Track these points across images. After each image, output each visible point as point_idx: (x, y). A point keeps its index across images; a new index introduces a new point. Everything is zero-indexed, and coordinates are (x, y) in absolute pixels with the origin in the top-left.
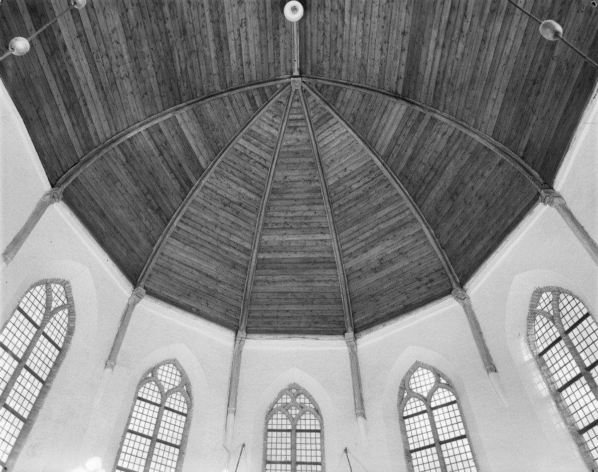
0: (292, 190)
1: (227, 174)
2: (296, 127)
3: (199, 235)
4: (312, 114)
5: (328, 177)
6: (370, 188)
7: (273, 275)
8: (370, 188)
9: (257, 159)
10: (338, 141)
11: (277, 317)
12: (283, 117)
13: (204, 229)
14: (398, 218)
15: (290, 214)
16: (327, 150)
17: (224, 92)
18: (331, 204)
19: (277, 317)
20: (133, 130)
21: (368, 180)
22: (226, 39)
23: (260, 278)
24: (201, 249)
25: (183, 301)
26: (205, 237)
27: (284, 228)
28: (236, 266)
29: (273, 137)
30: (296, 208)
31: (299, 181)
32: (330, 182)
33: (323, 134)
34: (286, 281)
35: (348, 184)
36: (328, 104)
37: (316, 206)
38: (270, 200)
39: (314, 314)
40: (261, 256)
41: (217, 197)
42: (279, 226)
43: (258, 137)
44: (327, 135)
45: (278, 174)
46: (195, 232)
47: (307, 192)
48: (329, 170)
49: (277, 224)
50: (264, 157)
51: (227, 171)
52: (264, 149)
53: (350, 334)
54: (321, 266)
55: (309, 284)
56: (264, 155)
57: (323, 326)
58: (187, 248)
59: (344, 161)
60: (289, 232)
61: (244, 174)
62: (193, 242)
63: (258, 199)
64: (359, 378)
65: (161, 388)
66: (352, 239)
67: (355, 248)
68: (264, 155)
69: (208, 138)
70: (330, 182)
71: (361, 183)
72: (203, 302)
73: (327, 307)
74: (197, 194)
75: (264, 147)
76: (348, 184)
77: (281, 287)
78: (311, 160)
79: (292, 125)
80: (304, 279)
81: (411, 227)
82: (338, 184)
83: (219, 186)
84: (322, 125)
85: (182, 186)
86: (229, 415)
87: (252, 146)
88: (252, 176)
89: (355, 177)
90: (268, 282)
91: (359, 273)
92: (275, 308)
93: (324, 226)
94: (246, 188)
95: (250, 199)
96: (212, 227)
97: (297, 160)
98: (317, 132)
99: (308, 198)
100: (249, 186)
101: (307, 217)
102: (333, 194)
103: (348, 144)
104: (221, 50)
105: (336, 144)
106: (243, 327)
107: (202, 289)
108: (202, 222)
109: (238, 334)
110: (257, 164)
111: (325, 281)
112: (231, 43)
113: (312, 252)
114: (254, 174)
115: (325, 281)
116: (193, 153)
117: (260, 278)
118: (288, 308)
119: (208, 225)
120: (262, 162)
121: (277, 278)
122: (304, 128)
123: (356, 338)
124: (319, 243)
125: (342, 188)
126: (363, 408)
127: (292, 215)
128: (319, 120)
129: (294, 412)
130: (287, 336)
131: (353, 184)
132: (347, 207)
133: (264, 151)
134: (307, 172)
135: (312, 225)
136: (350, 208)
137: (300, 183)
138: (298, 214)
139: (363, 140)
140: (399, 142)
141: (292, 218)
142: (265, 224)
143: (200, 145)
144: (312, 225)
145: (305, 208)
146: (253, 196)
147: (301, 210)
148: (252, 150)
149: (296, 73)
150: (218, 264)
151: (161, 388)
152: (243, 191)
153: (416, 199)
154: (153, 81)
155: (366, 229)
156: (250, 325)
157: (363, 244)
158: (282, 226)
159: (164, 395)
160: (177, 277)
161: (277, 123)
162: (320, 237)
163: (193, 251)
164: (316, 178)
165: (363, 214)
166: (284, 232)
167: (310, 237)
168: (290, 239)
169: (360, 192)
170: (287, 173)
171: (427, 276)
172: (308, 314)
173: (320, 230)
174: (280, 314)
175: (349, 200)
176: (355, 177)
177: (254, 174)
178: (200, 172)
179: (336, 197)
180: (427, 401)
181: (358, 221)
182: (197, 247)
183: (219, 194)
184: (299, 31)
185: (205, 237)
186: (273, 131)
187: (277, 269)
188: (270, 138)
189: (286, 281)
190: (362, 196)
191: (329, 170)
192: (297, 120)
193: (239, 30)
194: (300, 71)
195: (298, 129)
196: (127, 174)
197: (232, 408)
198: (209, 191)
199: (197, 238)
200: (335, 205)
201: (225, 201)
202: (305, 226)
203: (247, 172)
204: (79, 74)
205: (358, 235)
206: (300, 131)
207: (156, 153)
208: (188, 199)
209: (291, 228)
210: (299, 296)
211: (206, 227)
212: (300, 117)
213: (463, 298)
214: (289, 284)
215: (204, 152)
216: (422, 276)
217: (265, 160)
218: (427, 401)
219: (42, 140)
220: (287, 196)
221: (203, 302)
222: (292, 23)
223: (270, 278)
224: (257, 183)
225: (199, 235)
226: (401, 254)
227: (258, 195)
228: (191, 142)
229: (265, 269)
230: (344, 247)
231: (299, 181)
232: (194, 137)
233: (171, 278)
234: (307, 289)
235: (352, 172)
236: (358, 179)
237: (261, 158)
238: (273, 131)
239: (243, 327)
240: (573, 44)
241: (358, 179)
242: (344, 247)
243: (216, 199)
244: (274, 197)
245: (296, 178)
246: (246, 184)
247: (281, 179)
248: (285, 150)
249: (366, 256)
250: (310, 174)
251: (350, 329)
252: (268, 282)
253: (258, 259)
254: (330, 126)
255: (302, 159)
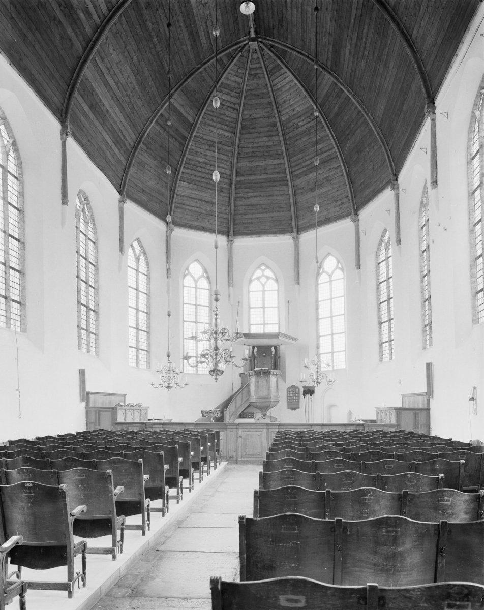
0: (256, 125)
1: (208, 121)
2: (256, 74)
3: (197, 174)
4: (267, 63)
5: (282, 114)
6: (310, 127)
7: (247, 193)
8: (310, 127)
9: (228, 104)
10: (288, 87)
11: (252, 223)
12: (245, 68)
13: (199, 169)
14: (328, 153)
15: (255, 145)
16: (280, 93)
17: (201, 67)
18: (284, 135)
19: (252, 223)
20: (147, 130)
21: (309, 120)
22: (197, 33)
23: (239, 195)
24: (199, 184)
25: (195, 223)
26: (200, 175)
27: (252, 156)
28: (223, 190)
29: (239, 84)
30: (260, 140)
31: (260, 118)
32: (284, 119)
33: (277, 80)
34: (255, 197)
35: (295, 121)
36: (279, 59)
37: (274, 137)
38: (241, 134)
39: (274, 219)
40: (238, 179)
41: (205, 142)
42: (249, 155)
43: (227, 87)
44: (280, 80)
45: (245, 113)
46: (194, 172)
47: (268, 126)
48: (282, 109)
49: (247, 153)
50: (233, 101)
51: (208, 119)
52: (232, 95)
53: (295, 234)
54: (278, 184)
55: (271, 198)
56: (234, 100)
57: (279, 227)
58: (191, 185)
59: (293, 102)
60: (257, 159)
61: (221, 119)
62: (194, 180)
63: (233, 135)
64: (298, 258)
65: (193, 278)
66: (299, 164)
67: (300, 171)
68: (234, 100)
69: (192, 102)
70: (284, 119)
71: (305, 122)
72: (206, 221)
73: (281, 214)
74: (191, 145)
75: (233, 94)
76: (295, 121)
77: (251, 201)
78: (268, 100)
79: (253, 73)
80: (268, 194)
81: (336, 162)
82: (289, 120)
83: (204, 133)
84: (275, 72)
85: (180, 143)
86: (230, 287)
87: (224, 95)
88: (226, 118)
89: (301, 116)
90: (244, 198)
91: (302, 190)
92: (250, 216)
93: (279, 152)
94: (223, 129)
95: (227, 137)
96: (204, 165)
97: (259, 101)
98: (273, 78)
99: (268, 131)
100: (225, 127)
101: (267, 146)
102: (285, 128)
103: (295, 89)
104: (194, 41)
105: (287, 88)
106: (232, 233)
107: (204, 212)
108: (197, 163)
109: (229, 239)
110: (229, 109)
111: (281, 195)
112: (202, 33)
113: (272, 173)
114: (227, 116)
115: (281, 195)
116: (184, 117)
117: (239, 195)
118: (258, 216)
119: (200, 165)
120: (233, 106)
121: (249, 195)
122: (262, 75)
123: (298, 235)
124: (276, 166)
125: (291, 124)
126: (299, 280)
127: (257, 145)
128: (274, 68)
129: (263, 280)
130: (258, 236)
131: (299, 122)
132: (295, 139)
133: (233, 97)
134: (267, 110)
135: (271, 152)
136: (297, 140)
137: (262, 119)
138: (262, 144)
139: (306, 90)
140: (330, 100)
141: (257, 147)
142: (239, 154)
143: (188, 109)
144: (271, 152)
145: (266, 139)
146: (228, 134)
147: (264, 141)
148: (224, 98)
149: (253, 35)
150: (211, 191)
151: (193, 278)
152: (221, 132)
153: (340, 142)
154: (154, 89)
155: (307, 158)
156: (236, 230)
157: (305, 169)
158: (251, 155)
159: (196, 282)
160: (187, 207)
161: (241, 73)
162: (276, 161)
163: (195, 186)
164: (273, 115)
165: (305, 147)
166: (252, 159)
167: (270, 162)
168: (257, 164)
169: (304, 128)
170: (252, 112)
171: (340, 200)
172: (271, 219)
173: (277, 156)
174: (253, 220)
175: (297, 134)
176: (301, 116)
177: (227, 116)
178: (191, 127)
179: (287, 131)
180: (330, 276)
181: (302, 151)
182: (197, 183)
183: (205, 139)
184: (255, 20)
185: (200, 175)
186: (239, 80)
187: (249, 188)
188: (237, 86)
189: (255, 197)
190: (305, 131)
191: (282, 109)
192: (256, 68)
193: (206, 23)
194: (256, 32)
195: (257, 76)
196: (148, 156)
197: (231, 284)
198: (198, 139)
199: (196, 176)
200: (287, 137)
201: (209, 143)
202: (266, 154)
203: (222, 117)
204: (116, 119)
205: (302, 161)
206: (259, 77)
207: (162, 131)
208: (186, 151)
209: (257, 156)
210: (264, 207)
211: (200, 167)
212: (258, 65)
213: (356, 220)
214: (258, 199)
215: (191, 112)
216: (338, 199)
217: (234, 104)
218: (330, 276)
219: (110, 173)
220: (252, 131)
221: (206, 221)
222: (247, 16)
223: (245, 195)
224: (231, 123)
225: (197, 174)
226: (327, 181)
227: (232, 132)
228: (182, 110)
229: (242, 188)
230: (293, 170)
231: (260, 118)
232: (182, 106)
233: (185, 210)
234: (269, 202)
235: (299, 112)
236: (303, 118)
237: (231, 103)
238: (239, 80)
239: (232, 233)
240: (388, 169)
241: (303, 118)
242: (293, 170)
243: (203, 144)
244: (244, 132)
245: (258, 116)
246: (223, 126)
247: (247, 117)
248: (249, 93)
249: (306, 178)
250: (268, 112)
251: (295, 230)
252: (244, 198)
253: (236, 181)
254: (282, 74)
255: (262, 100)
